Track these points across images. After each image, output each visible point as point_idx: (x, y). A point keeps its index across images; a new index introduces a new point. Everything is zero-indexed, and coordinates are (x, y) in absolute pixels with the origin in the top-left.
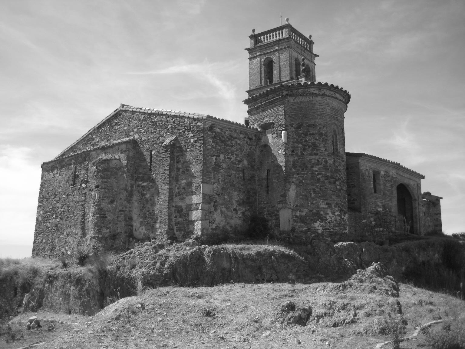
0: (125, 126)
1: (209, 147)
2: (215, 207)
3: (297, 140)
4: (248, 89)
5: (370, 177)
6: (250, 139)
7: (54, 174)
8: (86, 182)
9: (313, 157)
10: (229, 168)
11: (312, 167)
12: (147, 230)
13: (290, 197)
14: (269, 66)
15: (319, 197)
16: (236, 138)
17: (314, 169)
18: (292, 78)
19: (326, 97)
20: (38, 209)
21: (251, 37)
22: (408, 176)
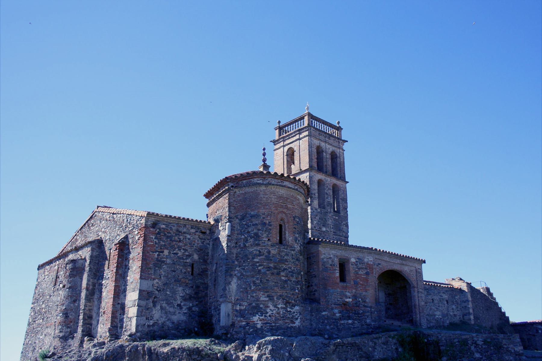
1: (150, 243)
2: (154, 303)
3: (241, 231)
5: (334, 265)
6: (204, 233)
7: (45, 276)
9: (255, 248)
10: (174, 264)
11: (253, 258)
13: (231, 290)
15: (260, 290)
16: (185, 233)
17: (256, 260)
19: (270, 186)
22: (398, 261)
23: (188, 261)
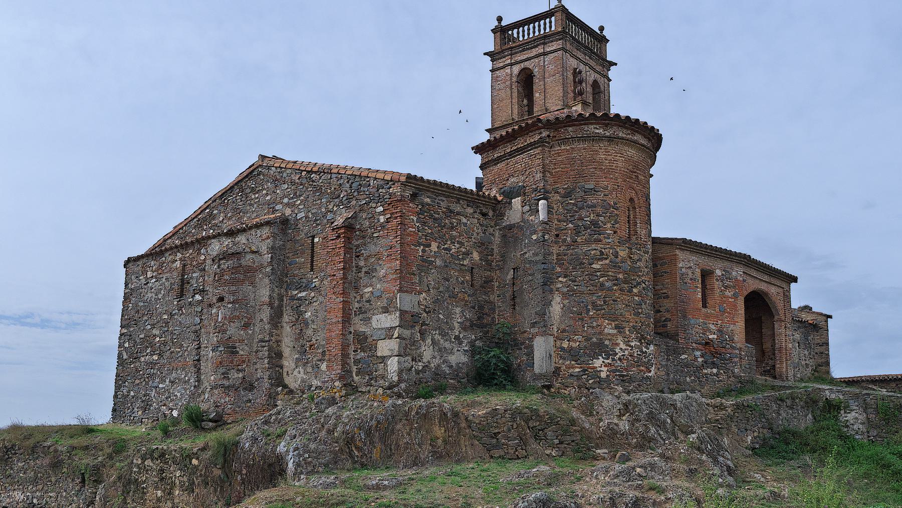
0: (267, 194)
2: (422, 333)
4: (490, 127)
7: (147, 279)
8: (202, 292)
12: (306, 373)
14: (527, 80)
16: (458, 214)
17: (594, 266)
18: (567, 106)
20: (120, 338)
21: (494, 31)
23: (465, 263)
